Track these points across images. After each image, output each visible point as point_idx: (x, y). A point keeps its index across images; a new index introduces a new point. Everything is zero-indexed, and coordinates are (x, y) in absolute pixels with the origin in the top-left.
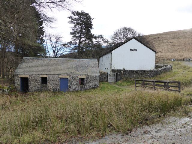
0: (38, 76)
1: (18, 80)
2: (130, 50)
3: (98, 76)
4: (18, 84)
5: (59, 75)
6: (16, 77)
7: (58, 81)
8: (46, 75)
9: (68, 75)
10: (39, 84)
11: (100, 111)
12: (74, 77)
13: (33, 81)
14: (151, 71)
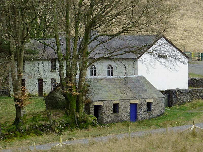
5: (129, 100)
7: (129, 107)
8: (118, 100)
12: (143, 101)
14: (185, 90)
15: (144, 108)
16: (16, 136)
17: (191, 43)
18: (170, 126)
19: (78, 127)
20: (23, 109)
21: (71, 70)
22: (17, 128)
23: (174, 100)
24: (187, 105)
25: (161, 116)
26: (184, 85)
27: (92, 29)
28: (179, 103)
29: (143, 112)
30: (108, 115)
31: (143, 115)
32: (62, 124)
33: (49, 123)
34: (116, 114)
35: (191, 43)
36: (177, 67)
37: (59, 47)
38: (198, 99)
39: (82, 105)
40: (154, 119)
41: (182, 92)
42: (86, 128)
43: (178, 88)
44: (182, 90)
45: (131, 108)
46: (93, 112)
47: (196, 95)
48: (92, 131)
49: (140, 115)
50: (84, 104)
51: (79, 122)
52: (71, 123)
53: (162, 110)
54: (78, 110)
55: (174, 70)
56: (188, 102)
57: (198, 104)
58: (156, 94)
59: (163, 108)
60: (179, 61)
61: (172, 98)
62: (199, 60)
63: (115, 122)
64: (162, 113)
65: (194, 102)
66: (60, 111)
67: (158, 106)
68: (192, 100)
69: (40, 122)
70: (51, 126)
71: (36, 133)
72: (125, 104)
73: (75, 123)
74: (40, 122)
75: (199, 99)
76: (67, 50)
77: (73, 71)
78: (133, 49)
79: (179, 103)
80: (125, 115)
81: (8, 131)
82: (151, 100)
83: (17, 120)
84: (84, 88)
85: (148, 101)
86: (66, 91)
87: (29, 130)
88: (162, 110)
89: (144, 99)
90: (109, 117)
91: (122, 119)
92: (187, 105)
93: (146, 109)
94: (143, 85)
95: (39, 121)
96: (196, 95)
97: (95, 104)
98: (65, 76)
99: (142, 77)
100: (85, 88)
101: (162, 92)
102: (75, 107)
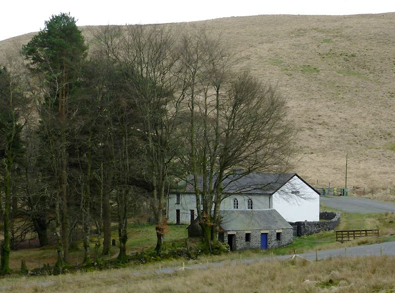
15: (274, 238)
16: (156, 260)
17: (338, 180)
18: (264, 253)
19: (212, 253)
20: (163, 237)
21: (206, 204)
22: (158, 253)
23: (303, 230)
25: (290, 244)
26: (316, 218)
30: (240, 243)
31: (272, 244)
32: (198, 250)
33: (186, 249)
34: (248, 242)
35: (338, 180)
36: (299, 203)
37: (197, 184)
39: (216, 234)
41: (309, 224)
42: (219, 254)
43: (306, 221)
45: (261, 237)
47: (324, 227)
48: (223, 256)
49: (270, 244)
50: (218, 233)
51: (213, 249)
52: (206, 249)
54: (212, 238)
55: (296, 204)
57: (324, 235)
58: (286, 225)
60: (301, 197)
61: (301, 229)
62: (341, 195)
65: (321, 233)
66: (198, 239)
67: (286, 236)
69: (179, 248)
70: (188, 251)
71: (175, 257)
73: (209, 249)
74: (179, 248)
75: (326, 230)
76: (204, 186)
77: (209, 205)
78: (260, 187)
81: (150, 255)
82: (249, 232)
83: (158, 246)
84: (218, 220)
85: (277, 231)
86: (202, 221)
87: (168, 255)
89: (273, 230)
92: (315, 236)
93: (275, 238)
94: (274, 218)
95: (178, 247)
96: (324, 227)
97: (229, 233)
98: (202, 209)
99: (275, 210)
100: (219, 219)
101: (292, 224)
102: (209, 236)
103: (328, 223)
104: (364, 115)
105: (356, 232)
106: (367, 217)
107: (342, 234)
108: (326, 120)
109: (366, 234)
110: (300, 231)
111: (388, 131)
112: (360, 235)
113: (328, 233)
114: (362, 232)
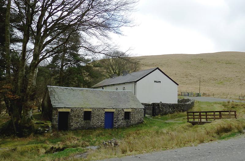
0: (82, 109)
1: (56, 116)
2: (155, 81)
3: (143, 109)
4: (57, 120)
5: (105, 108)
6: (54, 112)
7: (103, 115)
8: (90, 108)
9: (114, 109)
10: (81, 120)
11: (75, 133)
12: (120, 110)
13: (75, 116)
14: (175, 104)
15: (121, 117)
23: (157, 111)
24: (168, 116)
27: (47, 46)
28: (161, 113)
29: (120, 120)
34: (88, 121)
38: (179, 112)
40: (131, 126)
44: (165, 104)
46: (56, 119)
47: (178, 108)
53: (141, 119)
56: (170, 113)
59: (142, 117)
63: (85, 128)
64: (141, 122)
65: (176, 113)
68: (174, 112)
72: (99, 112)
75: (180, 111)
79: (161, 113)
80: (98, 123)
85: (125, 110)
88: (141, 119)
90: (78, 124)
91: (95, 126)
103: (182, 105)
104: (207, 74)
105: (208, 114)
106: (214, 104)
107: (194, 115)
108: (193, 75)
109: (220, 115)
110: (155, 112)
111: (216, 78)
112: (213, 117)
113: (181, 113)
114: (216, 113)
